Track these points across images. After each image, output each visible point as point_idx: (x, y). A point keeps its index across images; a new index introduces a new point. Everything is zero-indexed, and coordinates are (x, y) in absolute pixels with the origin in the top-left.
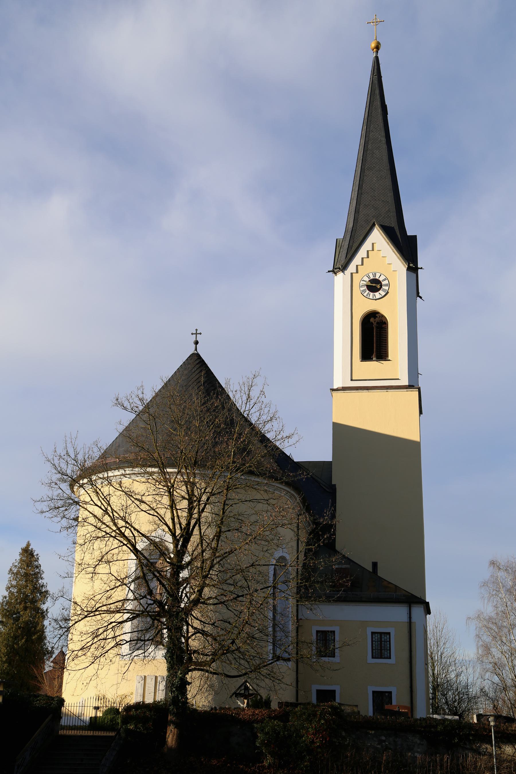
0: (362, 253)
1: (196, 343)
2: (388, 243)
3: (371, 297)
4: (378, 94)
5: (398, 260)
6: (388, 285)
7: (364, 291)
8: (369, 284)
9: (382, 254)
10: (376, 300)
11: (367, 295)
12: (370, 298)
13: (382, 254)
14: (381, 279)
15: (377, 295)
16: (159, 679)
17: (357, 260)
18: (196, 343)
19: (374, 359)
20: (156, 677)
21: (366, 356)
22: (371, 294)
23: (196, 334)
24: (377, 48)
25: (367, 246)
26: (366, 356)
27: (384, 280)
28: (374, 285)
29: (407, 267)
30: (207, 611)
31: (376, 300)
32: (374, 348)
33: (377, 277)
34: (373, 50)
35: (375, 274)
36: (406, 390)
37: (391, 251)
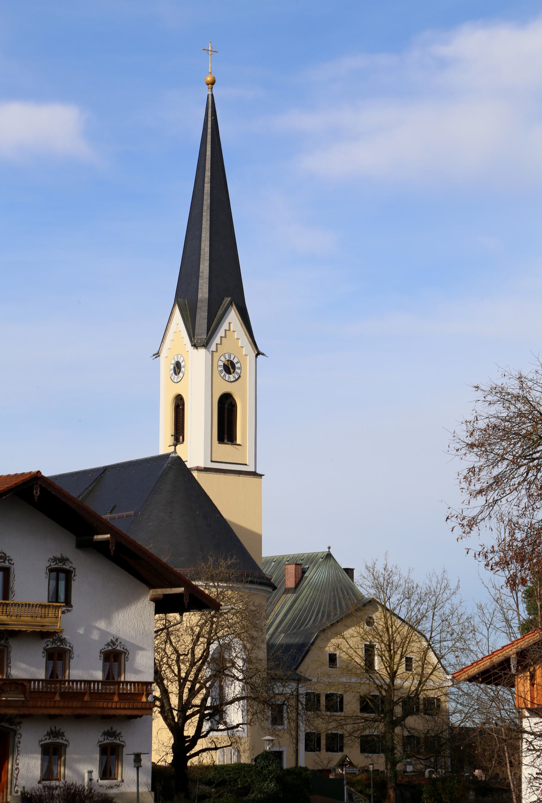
0: (221, 333)
2: (241, 324)
3: (227, 379)
5: (249, 345)
6: (240, 368)
11: (224, 376)
14: (237, 365)
17: (217, 340)
19: (226, 441)
21: (221, 440)
24: (213, 83)
25: (225, 326)
26: (221, 440)
33: (232, 359)
35: (230, 355)
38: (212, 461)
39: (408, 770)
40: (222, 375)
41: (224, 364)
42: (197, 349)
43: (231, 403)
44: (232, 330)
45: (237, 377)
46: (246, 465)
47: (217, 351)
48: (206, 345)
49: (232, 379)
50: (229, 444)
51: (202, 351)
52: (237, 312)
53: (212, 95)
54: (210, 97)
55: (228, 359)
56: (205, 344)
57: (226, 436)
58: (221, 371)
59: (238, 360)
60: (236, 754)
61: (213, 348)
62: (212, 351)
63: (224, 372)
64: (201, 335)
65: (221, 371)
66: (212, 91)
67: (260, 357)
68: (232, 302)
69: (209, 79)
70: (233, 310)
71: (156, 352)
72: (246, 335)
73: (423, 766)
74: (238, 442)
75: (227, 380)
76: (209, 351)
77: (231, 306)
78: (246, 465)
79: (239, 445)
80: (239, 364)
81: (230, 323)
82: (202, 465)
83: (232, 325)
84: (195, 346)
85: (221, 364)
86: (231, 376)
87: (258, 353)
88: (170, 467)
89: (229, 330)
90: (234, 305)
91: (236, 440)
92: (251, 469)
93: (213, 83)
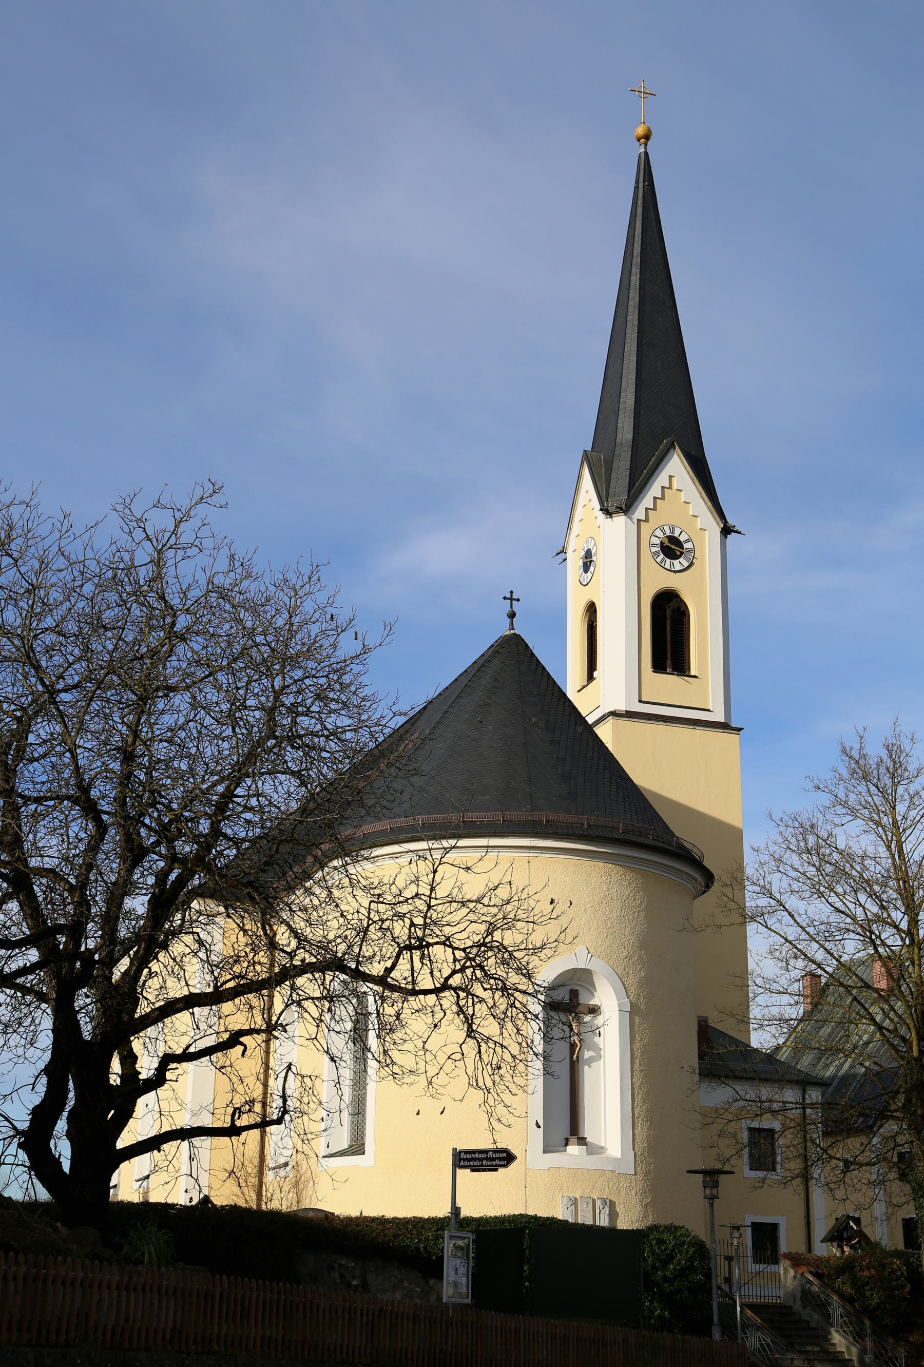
0: (654, 490)
1: (512, 615)
2: (693, 480)
3: (667, 566)
4: (653, 218)
5: (708, 513)
6: (693, 550)
7: (656, 553)
8: (666, 543)
9: (683, 497)
10: (676, 572)
11: (662, 561)
12: (666, 567)
13: (683, 497)
14: (682, 538)
15: (677, 564)
16: (599, 1203)
17: (647, 501)
18: (512, 615)
19: (668, 670)
20: (594, 1202)
21: (659, 666)
22: (668, 561)
23: (511, 599)
24: (647, 137)
25: (661, 480)
26: (659, 666)
27: (687, 541)
28: (673, 547)
29: (722, 526)
30: (59, 786)
31: (676, 572)
32: (666, 652)
33: (676, 535)
34: (639, 140)
35: (674, 529)
36: (692, 727)
37: (698, 495)
38: (640, 701)
39: (89, 941)
40: (659, 560)
41: (661, 542)
42: (611, 517)
43: (679, 608)
44: (675, 486)
45: (686, 564)
46: (709, 710)
47: (647, 520)
48: (626, 509)
49: (678, 567)
50: (673, 674)
51: (620, 520)
52: (683, 459)
53: (646, 153)
54: (643, 156)
55: (668, 533)
56: (624, 507)
57: (669, 662)
58: (656, 554)
59: (688, 537)
60: (607, 1210)
61: (639, 513)
62: (639, 520)
63: (662, 556)
64: (619, 496)
65: (656, 554)
66: (646, 148)
67: (732, 537)
68: (673, 443)
69: (641, 130)
70: (675, 455)
71: (560, 549)
72: (702, 497)
73: (417, 929)
74: (692, 673)
75: (669, 568)
76: (631, 519)
77: (672, 450)
78: (709, 710)
79: (695, 677)
80: (691, 543)
81: (670, 477)
82: (622, 707)
83: (674, 480)
84: (608, 512)
85: (658, 541)
86: (676, 562)
87: (727, 531)
88: (497, 652)
89: (670, 488)
90: (677, 447)
91: (689, 669)
92: (720, 717)
93: (647, 137)
